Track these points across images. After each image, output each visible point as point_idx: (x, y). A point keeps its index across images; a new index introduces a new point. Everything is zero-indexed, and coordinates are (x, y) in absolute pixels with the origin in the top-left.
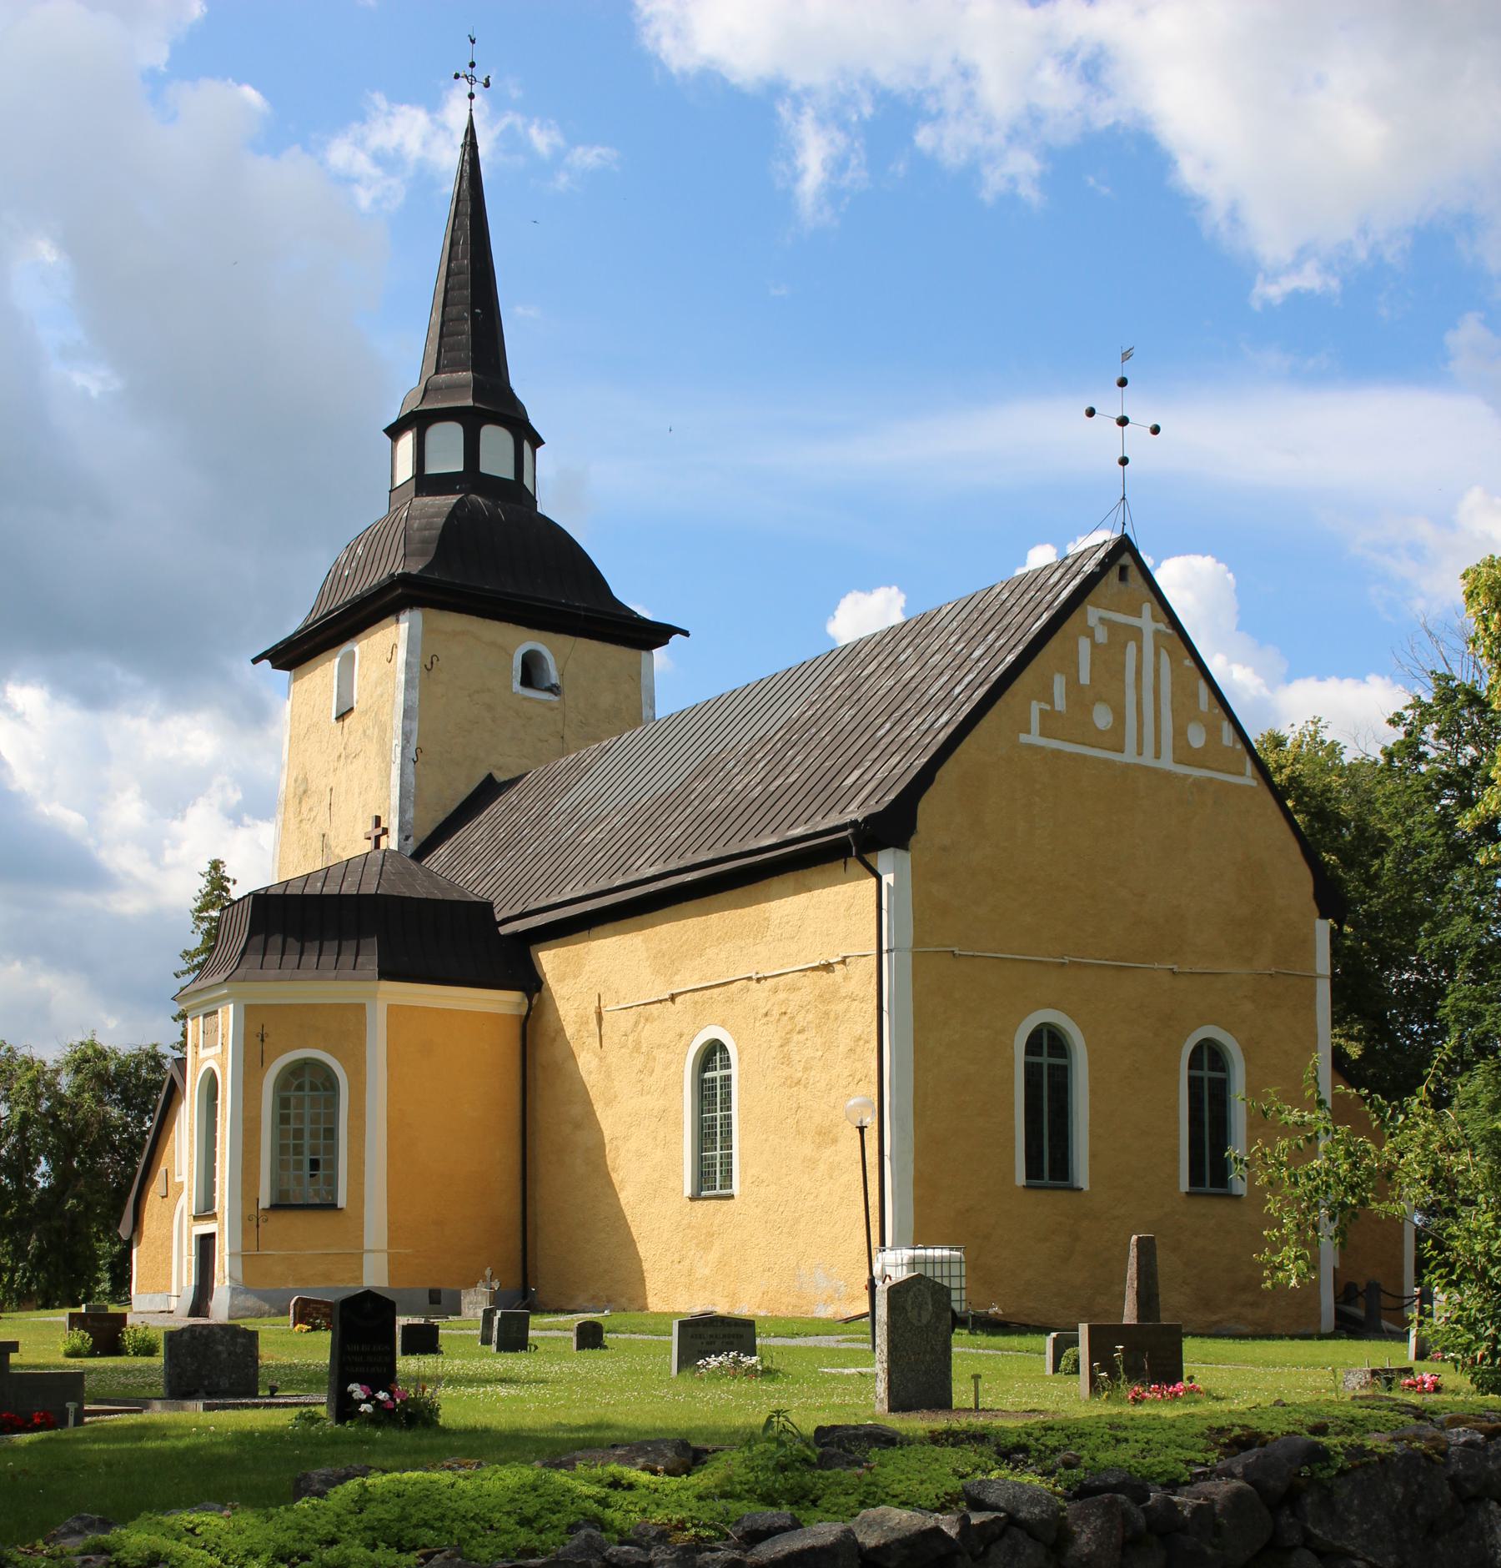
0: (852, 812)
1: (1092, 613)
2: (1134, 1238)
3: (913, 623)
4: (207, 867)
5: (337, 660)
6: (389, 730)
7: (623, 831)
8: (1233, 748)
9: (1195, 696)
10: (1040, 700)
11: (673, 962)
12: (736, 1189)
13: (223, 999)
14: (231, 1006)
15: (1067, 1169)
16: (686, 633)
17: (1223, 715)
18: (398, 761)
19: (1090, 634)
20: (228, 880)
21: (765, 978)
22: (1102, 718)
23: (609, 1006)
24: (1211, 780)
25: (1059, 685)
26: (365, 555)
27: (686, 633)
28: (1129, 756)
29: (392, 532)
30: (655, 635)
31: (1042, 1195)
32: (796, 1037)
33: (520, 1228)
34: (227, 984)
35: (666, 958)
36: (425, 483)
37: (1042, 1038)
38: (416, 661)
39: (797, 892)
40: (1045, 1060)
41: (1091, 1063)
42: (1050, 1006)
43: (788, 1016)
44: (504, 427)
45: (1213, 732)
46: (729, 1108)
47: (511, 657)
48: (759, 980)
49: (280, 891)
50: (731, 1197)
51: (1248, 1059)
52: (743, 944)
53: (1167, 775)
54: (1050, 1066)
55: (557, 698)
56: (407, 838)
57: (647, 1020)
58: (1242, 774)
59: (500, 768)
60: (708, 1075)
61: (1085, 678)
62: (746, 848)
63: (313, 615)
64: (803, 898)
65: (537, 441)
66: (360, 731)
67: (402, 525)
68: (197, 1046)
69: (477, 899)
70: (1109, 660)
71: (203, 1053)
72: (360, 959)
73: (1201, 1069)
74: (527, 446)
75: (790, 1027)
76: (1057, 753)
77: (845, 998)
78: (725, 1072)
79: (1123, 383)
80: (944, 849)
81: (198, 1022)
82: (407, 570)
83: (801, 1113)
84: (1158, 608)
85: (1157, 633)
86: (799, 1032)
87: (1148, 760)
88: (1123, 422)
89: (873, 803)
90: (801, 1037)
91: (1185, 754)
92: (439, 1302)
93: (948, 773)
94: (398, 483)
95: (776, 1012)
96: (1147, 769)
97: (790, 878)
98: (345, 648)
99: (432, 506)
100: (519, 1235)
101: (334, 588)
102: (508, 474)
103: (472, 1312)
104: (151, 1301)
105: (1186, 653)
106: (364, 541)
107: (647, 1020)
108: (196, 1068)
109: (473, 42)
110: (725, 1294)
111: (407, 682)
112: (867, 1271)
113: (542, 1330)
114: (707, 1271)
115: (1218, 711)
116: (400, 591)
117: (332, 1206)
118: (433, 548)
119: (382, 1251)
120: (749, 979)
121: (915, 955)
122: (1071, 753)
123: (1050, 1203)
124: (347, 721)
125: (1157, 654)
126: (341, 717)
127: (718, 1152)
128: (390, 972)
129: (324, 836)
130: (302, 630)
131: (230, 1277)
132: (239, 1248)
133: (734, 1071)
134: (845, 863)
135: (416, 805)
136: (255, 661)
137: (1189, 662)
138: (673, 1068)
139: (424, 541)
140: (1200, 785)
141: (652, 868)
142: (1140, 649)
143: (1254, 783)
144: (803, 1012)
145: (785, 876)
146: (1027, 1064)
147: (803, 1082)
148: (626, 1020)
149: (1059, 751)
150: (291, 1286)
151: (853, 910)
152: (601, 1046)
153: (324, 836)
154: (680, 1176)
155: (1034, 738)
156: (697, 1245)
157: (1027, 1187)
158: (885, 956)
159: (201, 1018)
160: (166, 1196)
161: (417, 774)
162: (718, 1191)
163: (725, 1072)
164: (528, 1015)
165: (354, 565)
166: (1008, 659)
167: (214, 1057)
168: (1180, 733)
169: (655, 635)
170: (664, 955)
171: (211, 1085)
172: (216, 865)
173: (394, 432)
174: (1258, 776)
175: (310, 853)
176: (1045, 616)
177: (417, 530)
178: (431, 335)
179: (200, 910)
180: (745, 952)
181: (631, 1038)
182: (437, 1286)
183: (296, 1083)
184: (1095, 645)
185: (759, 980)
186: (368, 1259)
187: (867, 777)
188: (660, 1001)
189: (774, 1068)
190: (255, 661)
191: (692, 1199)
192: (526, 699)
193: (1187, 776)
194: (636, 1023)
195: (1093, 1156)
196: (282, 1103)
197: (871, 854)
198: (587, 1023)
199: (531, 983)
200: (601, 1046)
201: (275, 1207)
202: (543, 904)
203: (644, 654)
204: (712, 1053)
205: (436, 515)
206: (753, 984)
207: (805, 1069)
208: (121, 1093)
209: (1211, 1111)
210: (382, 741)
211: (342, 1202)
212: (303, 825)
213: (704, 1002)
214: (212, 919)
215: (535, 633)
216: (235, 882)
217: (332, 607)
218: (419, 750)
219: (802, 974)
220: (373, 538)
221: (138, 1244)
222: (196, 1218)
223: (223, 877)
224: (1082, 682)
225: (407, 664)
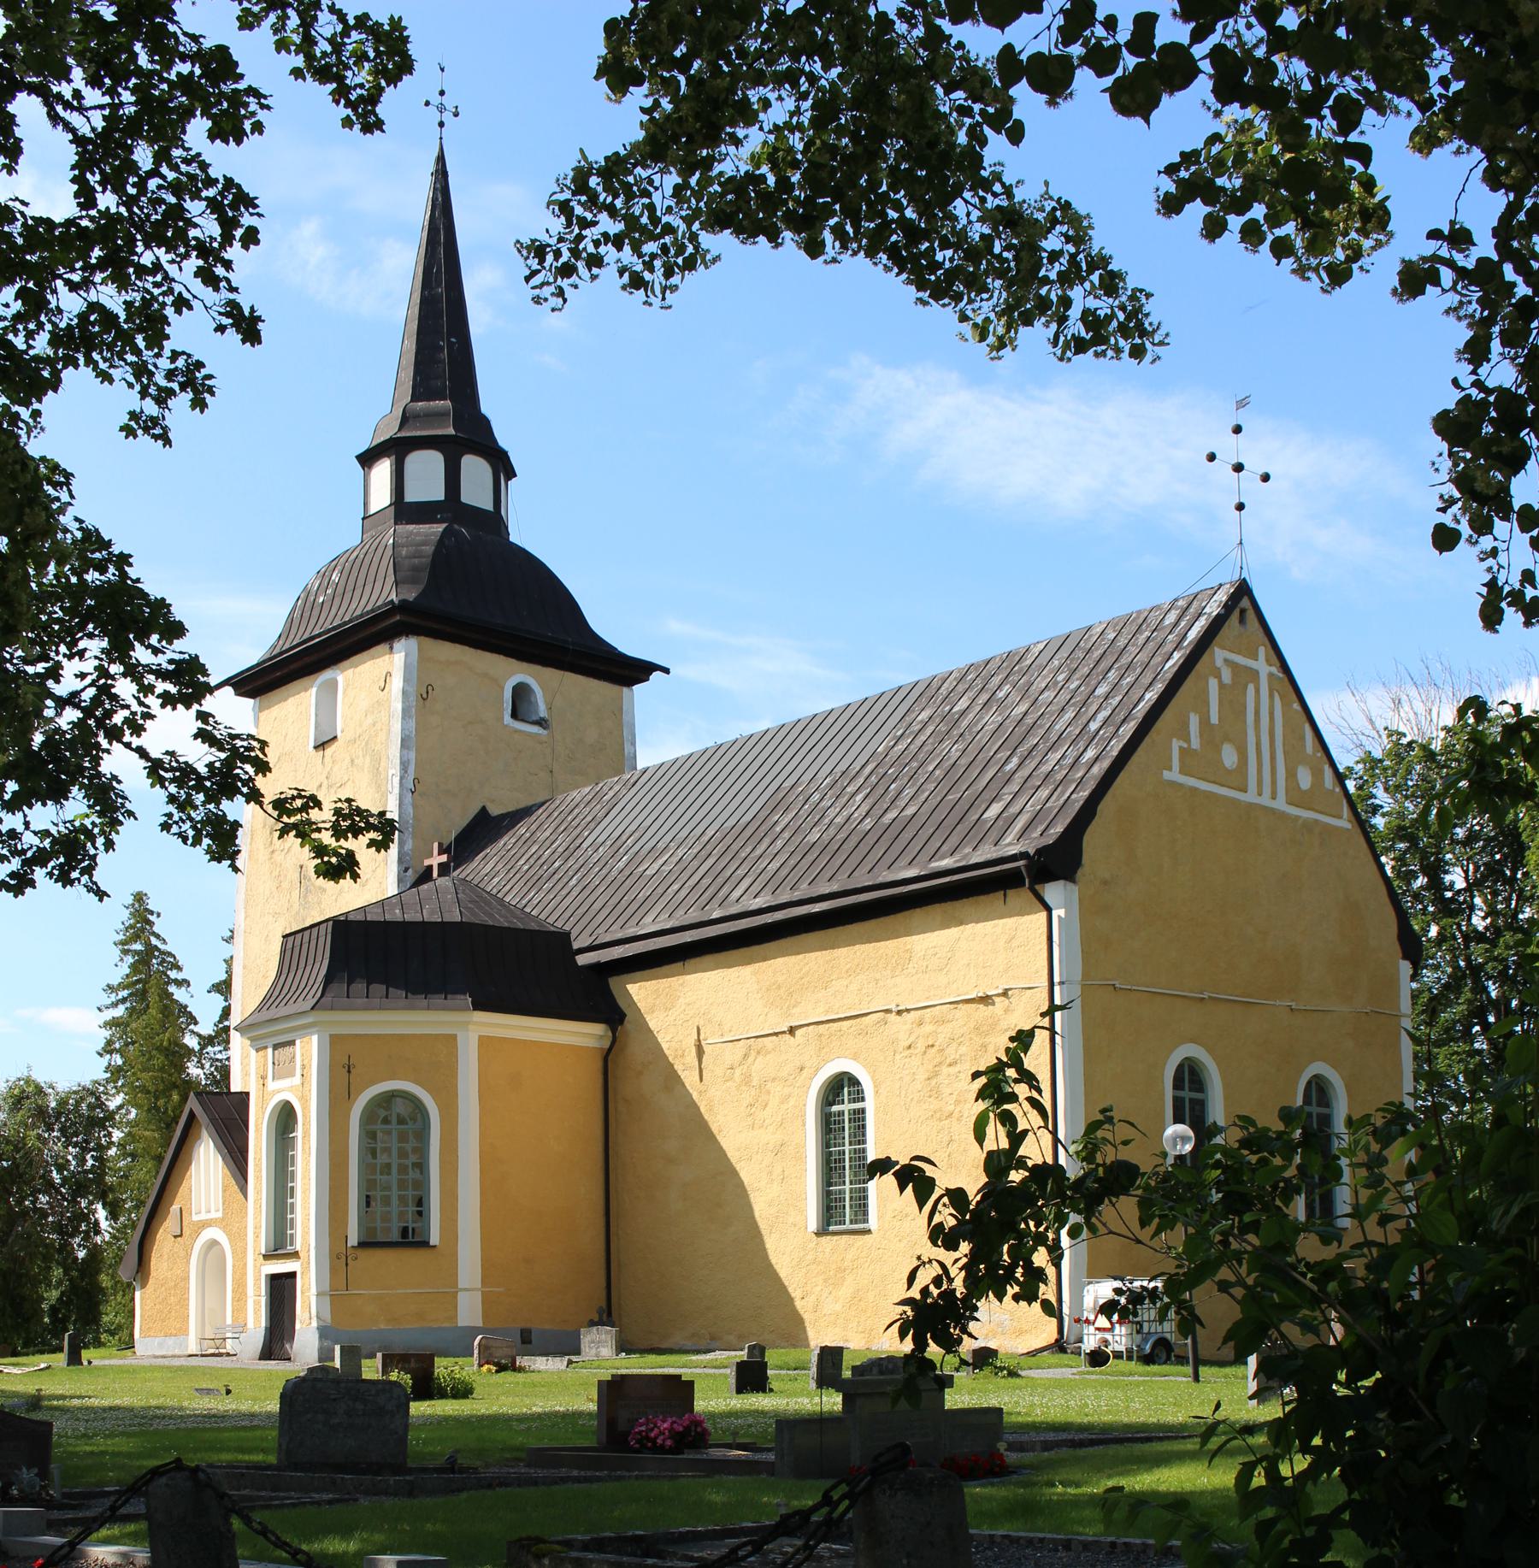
0: (1010, 844)
1: (1219, 654)
3: (998, 661)
4: (130, 900)
5: (314, 690)
6: (383, 760)
7: (696, 863)
8: (1333, 790)
9: (1302, 738)
10: (1179, 738)
11: (791, 995)
12: (873, 1222)
13: (305, 1029)
14: (315, 1038)
16: (666, 671)
17: (1325, 758)
18: (396, 790)
19: (1218, 676)
20: (152, 913)
21: (908, 1011)
22: (1229, 757)
23: (709, 1039)
24: (1316, 821)
26: (342, 583)
27: (666, 671)
28: (1250, 797)
29: (376, 560)
30: (635, 671)
32: (945, 1070)
33: (603, 1266)
34: (313, 1012)
35: (783, 989)
36: (404, 510)
38: (411, 690)
39: (945, 925)
41: (1226, 1098)
42: (1193, 1041)
43: (935, 1049)
44: (489, 462)
45: (1317, 774)
47: (502, 689)
49: (360, 917)
50: (869, 1232)
51: (1350, 1095)
52: (878, 976)
53: (1283, 816)
54: (1191, 1100)
55: (545, 732)
56: (406, 870)
57: (758, 1053)
58: (1340, 817)
59: (493, 801)
60: (835, 1108)
61: (1214, 719)
62: (880, 880)
63: (281, 642)
64: (953, 932)
66: (348, 760)
67: (389, 552)
68: (264, 1078)
69: (552, 929)
70: (1233, 699)
71: (271, 1085)
72: (329, 995)
75: (938, 1060)
76: (1194, 790)
78: (1180, 1093)
79: (1237, 430)
80: (1105, 883)
81: (266, 1056)
82: (402, 597)
83: (954, 1146)
84: (1272, 652)
85: (1271, 675)
86: (950, 1065)
87: (1265, 800)
88: (1238, 468)
89: (1036, 834)
90: (953, 1070)
91: (1297, 797)
92: (530, 1342)
93: (1106, 806)
94: (372, 510)
95: (921, 1046)
96: (1265, 808)
97: (936, 911)
98: (327, 675)
99: (418, 534)
100: (603, 1272)
101: (306, 615)
103: (594, 1351)
104: (160, 1345)
105: (1294, 697)
106: (339, 567)
107: (758, 1053)
108: (263, 1101)
109: (442, 70)
110: (860, 1329)
111: (403, 709)
113: (715, 1368)
114: (838, 1307)
116: (398, 618)
117: (425, 1244)
118: (425, 576)
119: (461, 1290)
120: (888, 1011)
121: (1083, 985)
122: (1205, 791)
124: (329, 751)
125: (1271, 696)
126: (321, 746)
128: (479, 1006)
129: (301, 867)
130: (270, 659)
131: (318, 1317)
132: (327, 1287)
133: (869, 1105)
134: (1005, 895)
135: (414, 836)
137: (1296, 706)
138: (792, 1102)
139: (415, 569)
140: (1309, 826)
141: (757, 900)
142: (1257, 691)
143: (1349, 826)
144: (955, 1045)
145: (930, 908)
147: (956, 1115)
148: (734, 1053)
150: (382, 1327)
151: (1015, 943)
152: (701, 1080)
153: (301, 867)
154: (803, 1212)
155: (1173, 775)
156: (825, 1281)
158: (1057, 989)
159: (270, 1050)
160: (181, 1235)
161: (414, 806)
162: (848, 1226)
164: (610, 1049)
165: (329, 591)
166: (1147, 696)
167: (291, 1089)
168: (1291, 775)
169: (635, 671)
170: (779, 987)
171: (286, 1117)
172: (140, 898)
173: (367, 459)
174: (1353, 819)
175: (285, 885)
176: (1176, 655)
177: (406, 557)
178: (404, 362)
179: (124, 943)
180: (881, 983)
181: (738, 1072)
182: (528, 1325)
184: (1222, 686)
185: (899, 1013)
186: (462, 1298)
187: (1014, 809)
188: (776, 1034)
189: (919, 1101)
191: (818, 1234)
192: (516, 731)
193: (1298, 818)
194: (746, 1056)
196: (368, 1135)
198: (683, 1056)
199: (613, 1014)
200: (701, 1080)
201: (362, 1245)
202: (619, 935)
203: (625, 690)
205: (425, 543)
206: (892, 1017)
207: (958, 1102)
208: (60, 1130)
210: (376, 771)
211: (434, 1239)
212: (275, 855)
213: (831, 1035)
214: (136, 952)
215: (525, 665)
216: (159, 915)
217: (305, 637)
218: (416, 780)
219: (952, 1006)
220: (349, 566)
221: (143, 1286)
222: (266, 1257)
223: (147, 910)
225: (404, 692)
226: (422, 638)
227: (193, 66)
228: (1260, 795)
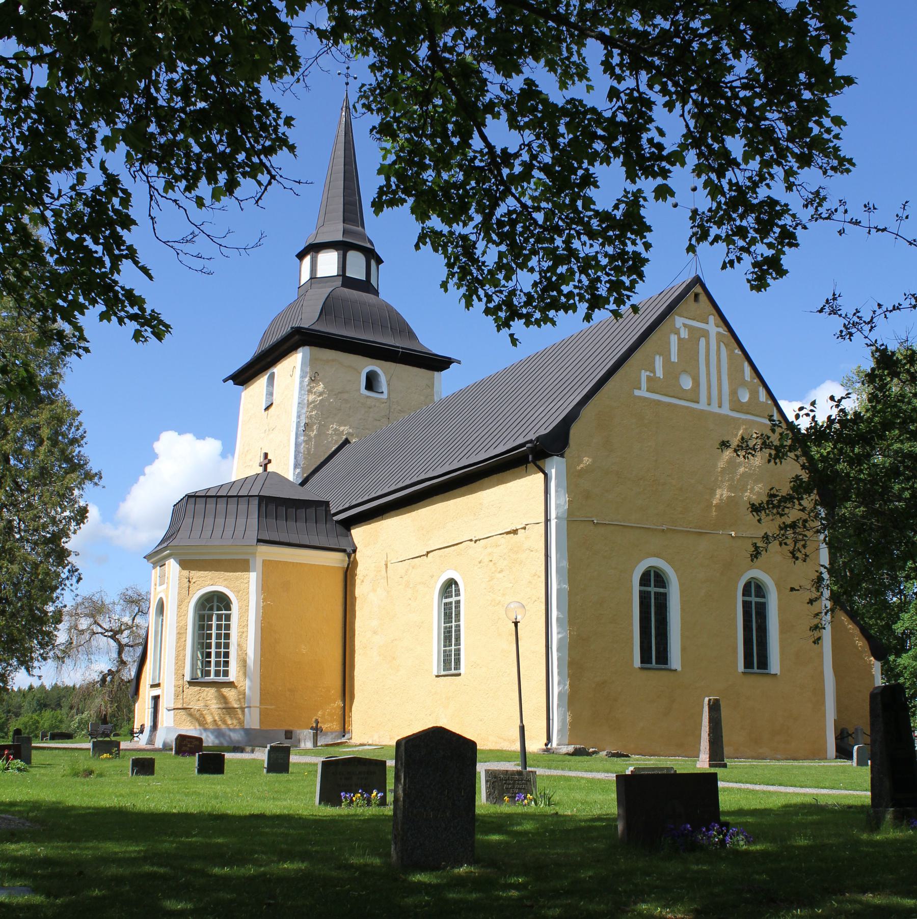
1: (679, 321)
2: (707, 699)
10: (646, 370)
12: (775, 664)
15: (837, 696)
16: (459, 362)
17: (760, 383)
19: (677, 333)
21: (480, 540)
25: (659, 362)
27: (459, 362)
28: (702, 406)
31: (651, 674)
37: (650, 575)
40: (652, 589)
45: (754, 394)
46: (459, 621)
48: (476, 541)
61: (674, 358)
65: (379, 261)
70: (689, 349)
73: (750, 596)
74: (373, 263)
77: (526, 550)
78: (457, 598)
85: (718, 333)
87: (714, 408)
90: (501, 575)
91: (737, 406)
93: (588, 412)
94: (302, 284)
102: (363, 277)
105: (736, 345)
112: (519, 721)
115: (756, 380)
120: (471, 540)
123: (655, 678)
126: (267, 409)
127: (453, 647)
133: (462, 598)
136: (225, 381)
137: (738, 351)
142: (708, 343)
146: (640, 591)
149: (659, 401)
155: (643, 393)
157: (642, 668)
162: (453, 672)
163: (457, 598)
168: (734, 393)
173: (301, 256)
183: (208, 606)
184: (679, 339)
185: (476, 541)
190: (225, 381)
192: (368, 397)
195: (684, 649)
197: (542, 461)
204: (450, 586)
209: (757, 622)
224: (672, 360)
226: (313, 348)
227: (707, 175)
228: (709, 404)
